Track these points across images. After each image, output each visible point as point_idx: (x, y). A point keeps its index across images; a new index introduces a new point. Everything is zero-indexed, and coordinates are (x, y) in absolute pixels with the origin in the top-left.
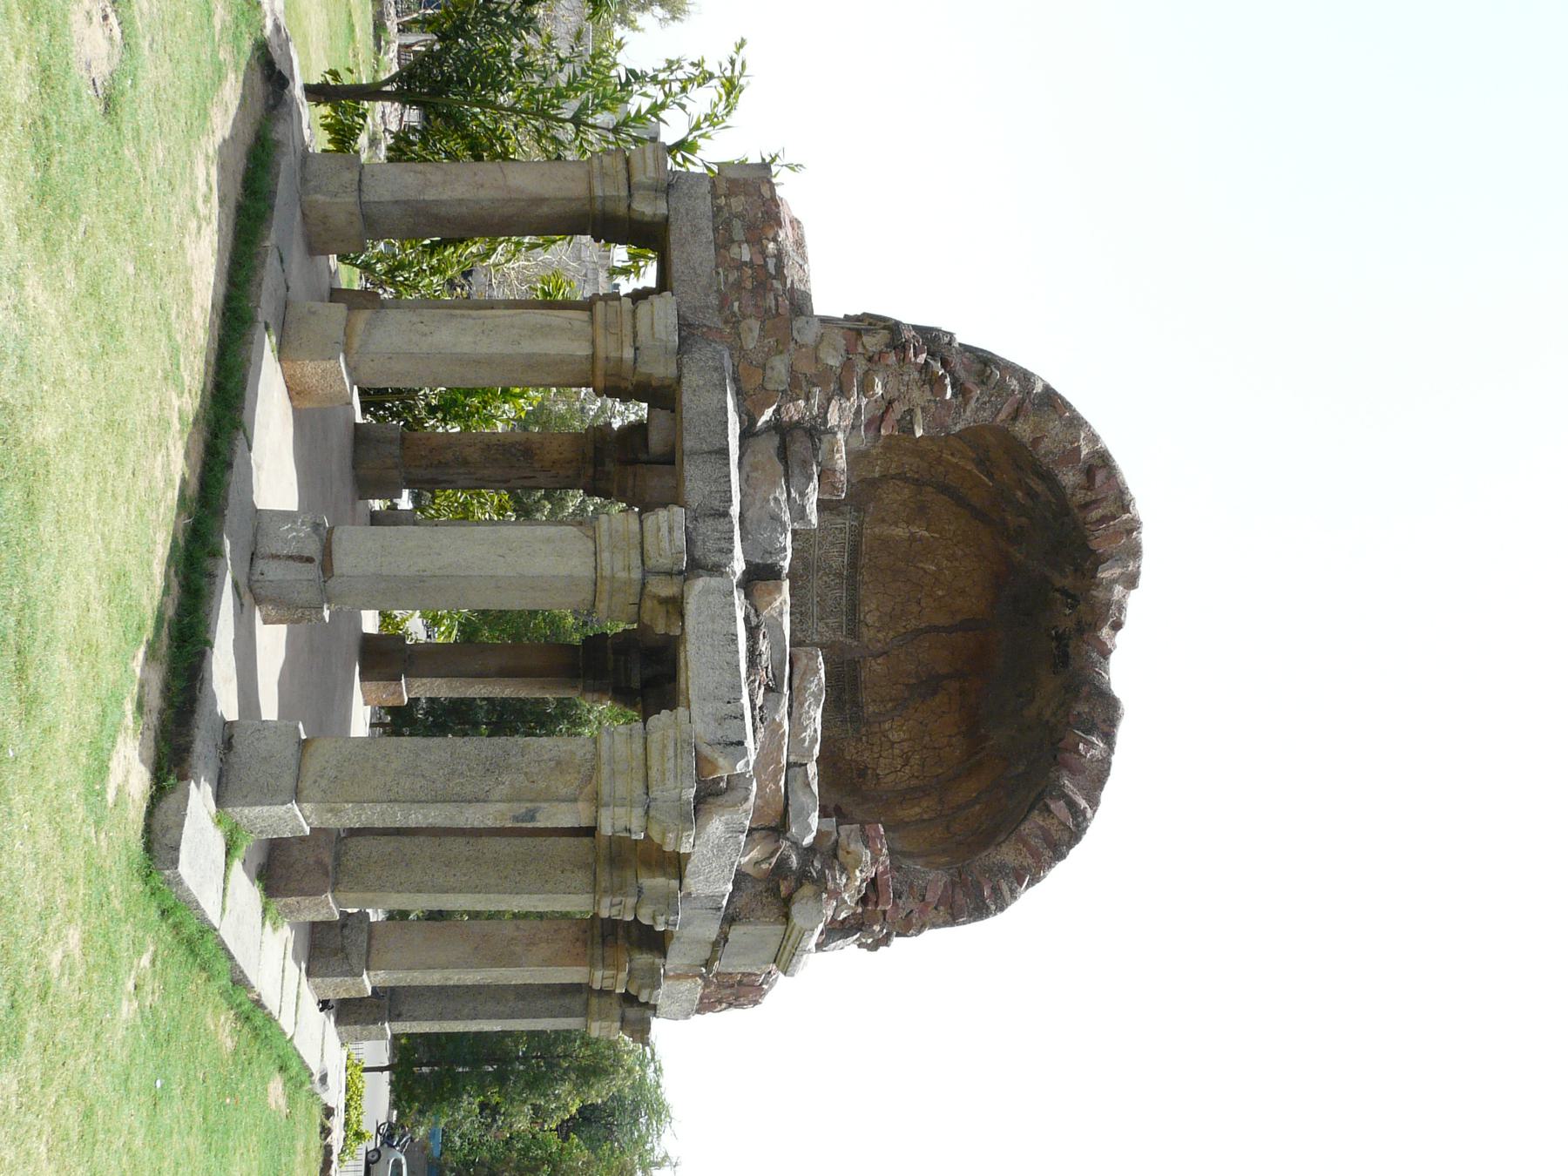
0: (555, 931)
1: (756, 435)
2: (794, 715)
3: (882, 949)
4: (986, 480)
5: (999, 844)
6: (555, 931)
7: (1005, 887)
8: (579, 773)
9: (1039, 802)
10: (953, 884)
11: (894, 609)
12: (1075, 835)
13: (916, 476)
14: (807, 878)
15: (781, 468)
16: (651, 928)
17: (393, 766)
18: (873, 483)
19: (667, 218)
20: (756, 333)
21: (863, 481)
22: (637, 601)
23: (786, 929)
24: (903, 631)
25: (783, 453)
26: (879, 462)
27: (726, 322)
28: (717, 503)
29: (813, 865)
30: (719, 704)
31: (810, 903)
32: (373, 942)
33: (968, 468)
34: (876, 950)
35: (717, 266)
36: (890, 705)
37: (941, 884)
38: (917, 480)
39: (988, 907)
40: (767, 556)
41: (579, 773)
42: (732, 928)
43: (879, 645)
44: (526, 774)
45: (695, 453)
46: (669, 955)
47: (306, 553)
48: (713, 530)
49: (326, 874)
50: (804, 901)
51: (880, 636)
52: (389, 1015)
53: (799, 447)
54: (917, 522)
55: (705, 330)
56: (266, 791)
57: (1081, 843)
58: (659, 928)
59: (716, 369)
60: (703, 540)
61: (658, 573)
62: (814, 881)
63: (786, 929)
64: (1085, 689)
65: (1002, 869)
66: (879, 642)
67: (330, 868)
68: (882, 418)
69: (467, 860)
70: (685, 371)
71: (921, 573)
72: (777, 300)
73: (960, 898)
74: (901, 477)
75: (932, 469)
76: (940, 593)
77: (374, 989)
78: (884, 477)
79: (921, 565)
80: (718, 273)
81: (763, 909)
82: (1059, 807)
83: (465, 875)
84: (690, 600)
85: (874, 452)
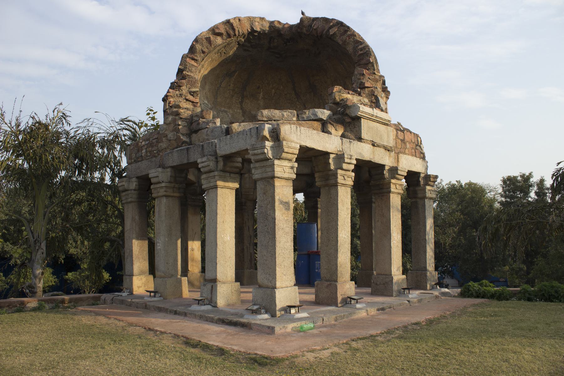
0: (379, 207)
1: (191, 141)
2: (278, 119)
3: (389, 89)
4: (237, 73)
5: (347, 51)
6: (379, 207)
7: (360, 47)
8: (266, 185)
9: (331, 38)
10: (359, 65)
11: (289, 103)
12: (340, 24)
13: (240, 98)
14: (344, 112)
15: (200, 131)
16: (355, 165)
17: (265, 253)
18: (244, 113)
19: (138, 178)
20: (162, 144)
21: (243, 116)
22: (229, 174)
23: (362, 118)
24: (296, 99)
25: (196, 132)
26: (236, 110)
27: (159, 154)
28: (200, 149)
29: (339, 111)
30: (247, 137)
31: (351, 110)
32: (382, 273)
33: (234, 80)
34: (389, 92)
35: (146, 160)
36: (321, 101)
37: (359, 69)
38: (242, 97)
39: (367, 51)
40: (223, 132)
41: (266, 185)
42: (363, 138)
43: (301, 107)
44: (267, 205)
45: (188, 159)
46: (384, 164)
47: (210, 288)
48: (207, 149)
49: (331, 284)
50: (351, 112)
51: (298, 107)
52: (425, 271)
53: (194, 126)
54: (258, 97)
55: (161, 161)
56: (271, 299)
57: (343, 21)
58: (355, 162)
59: (168, 155)
60: (209, 152)
61: (217, 166)
62: (345, 109)
63: (362, 118)
64: (299, 30)
65: (355, 49)
66: (300, 107)
67: (329, 283)
68: (193, 102)
69: (328, 233)
70: (169, 165)
71: (275, 94)
72: (154, 139)
73: (364, 62)
74: (241, 103)
75: (237, 92)
76: (282, 87)
77: (403, 274)
78: (242, 108)
79: (273, 94)
80: (148, 159)
81: (356, 127)
82: (332, 32)
83: (332, 234)
84: (222, 153)
85: (231, 112)
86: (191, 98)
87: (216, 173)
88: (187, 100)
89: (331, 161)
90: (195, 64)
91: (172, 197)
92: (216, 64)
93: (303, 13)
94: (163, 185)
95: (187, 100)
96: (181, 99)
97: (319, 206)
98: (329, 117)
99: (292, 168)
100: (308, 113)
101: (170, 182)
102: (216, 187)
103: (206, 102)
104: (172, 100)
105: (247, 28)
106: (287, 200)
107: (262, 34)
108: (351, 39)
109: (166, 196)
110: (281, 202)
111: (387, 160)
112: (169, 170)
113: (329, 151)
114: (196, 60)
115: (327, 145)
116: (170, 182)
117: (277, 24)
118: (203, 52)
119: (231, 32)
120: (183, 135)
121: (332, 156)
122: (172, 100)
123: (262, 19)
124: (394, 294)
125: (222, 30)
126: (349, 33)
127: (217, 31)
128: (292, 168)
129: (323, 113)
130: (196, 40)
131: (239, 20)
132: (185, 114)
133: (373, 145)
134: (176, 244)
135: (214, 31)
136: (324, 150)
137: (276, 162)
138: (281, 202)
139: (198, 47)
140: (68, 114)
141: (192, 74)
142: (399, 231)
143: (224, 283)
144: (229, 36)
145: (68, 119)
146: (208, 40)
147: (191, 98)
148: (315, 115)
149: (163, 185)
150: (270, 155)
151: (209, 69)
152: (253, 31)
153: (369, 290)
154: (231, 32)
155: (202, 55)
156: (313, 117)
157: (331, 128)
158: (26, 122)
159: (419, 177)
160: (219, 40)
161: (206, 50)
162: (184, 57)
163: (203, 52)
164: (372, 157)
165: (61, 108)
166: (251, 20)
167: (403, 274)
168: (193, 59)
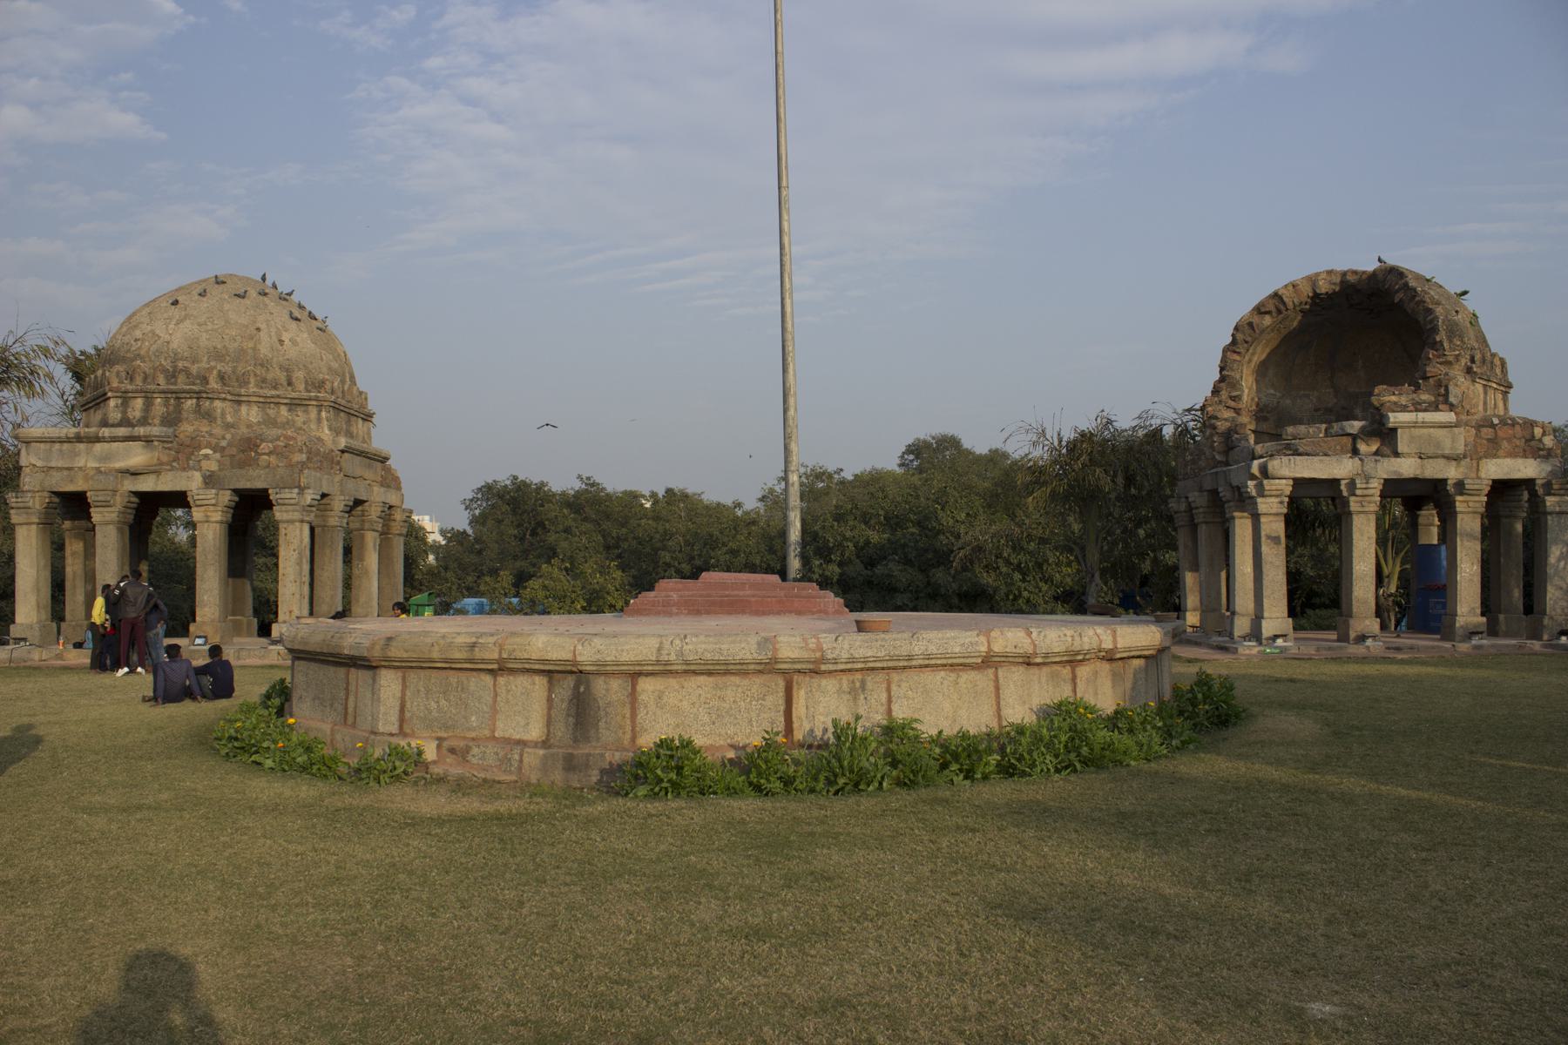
25: (1232, 448)
77: (1483, 614)
86: (1232, 404)
87: (1232, 504)
88: (1228, 407)
89: (1343, 487)
90: (1238, 358)
91: (1213, 522)
92: (1274, 344)
93: (1380, 260)
94: (1201, 510)
95: (1228, 407)
96: (1221, 407)
97: (1526, 505)
98: (1362, 429)
99: (1281, 503)
100: (1336, 427)
101: (1208, 507)
102: (1233, 518)
103: (1272, 391)
104: (1210, 409)
105: (1307, 291)
106: (1276, 535)
107: (1330, 296)
108: (1421, 307)
109: (1206, 523)
110: (1269, 537)
111: (1451, 473)
112: (1205, 493)
113: (1338, 477)
114: (1239, 353)
115: (1335, 471)
116: (1208, 507)
117: (1350, 278)
118: (1246, 342)
119: (1282, 307)
120: (1219, 453)
121: (1343, 482)
122: (1210, 409)
123: (1330, 272)
124: (1458, 638)
125: (1271, 307)
126: (1417, 299)
127: (1263, 310)
128: (1281, 503)
129: (1353, 426)
130: (1236, 328)
131: (1294, 286)
132: (1222, 426)
133: (1420, 458)
134: (1219, 575)
135: (1259, 310)
136: (1331, 477)
137: (1259, 500)
138: (1269, 537)
139: (1240, 336)
140: (1113, 418)
141: (1233, 374)
142: (1476, 561)
143: (1243, 615)
144: (1279, 312)
145: (1114, 424)
146: (1250, 325)
147: (1232, 404)
148: (1343, 429)
149: (1201, 510)
150: (1254, 493)
151: (1268, 350)
152: (1316, 295)
153: (1439, 637)
154: (1282, 307)
155: (1246, 345)
156: (1341, 432)
157: (1363, 447)
158: (1069, 435)
159: (1534, 485)
160: (1267, 320)
161: (1249, 339)
162: (1226, 350)
163: (1246, 342)
164: (1418, 472)
165: (1105, 414)
166: (1312, 280)
167: (1483, 614)
168: (1235, 352)
